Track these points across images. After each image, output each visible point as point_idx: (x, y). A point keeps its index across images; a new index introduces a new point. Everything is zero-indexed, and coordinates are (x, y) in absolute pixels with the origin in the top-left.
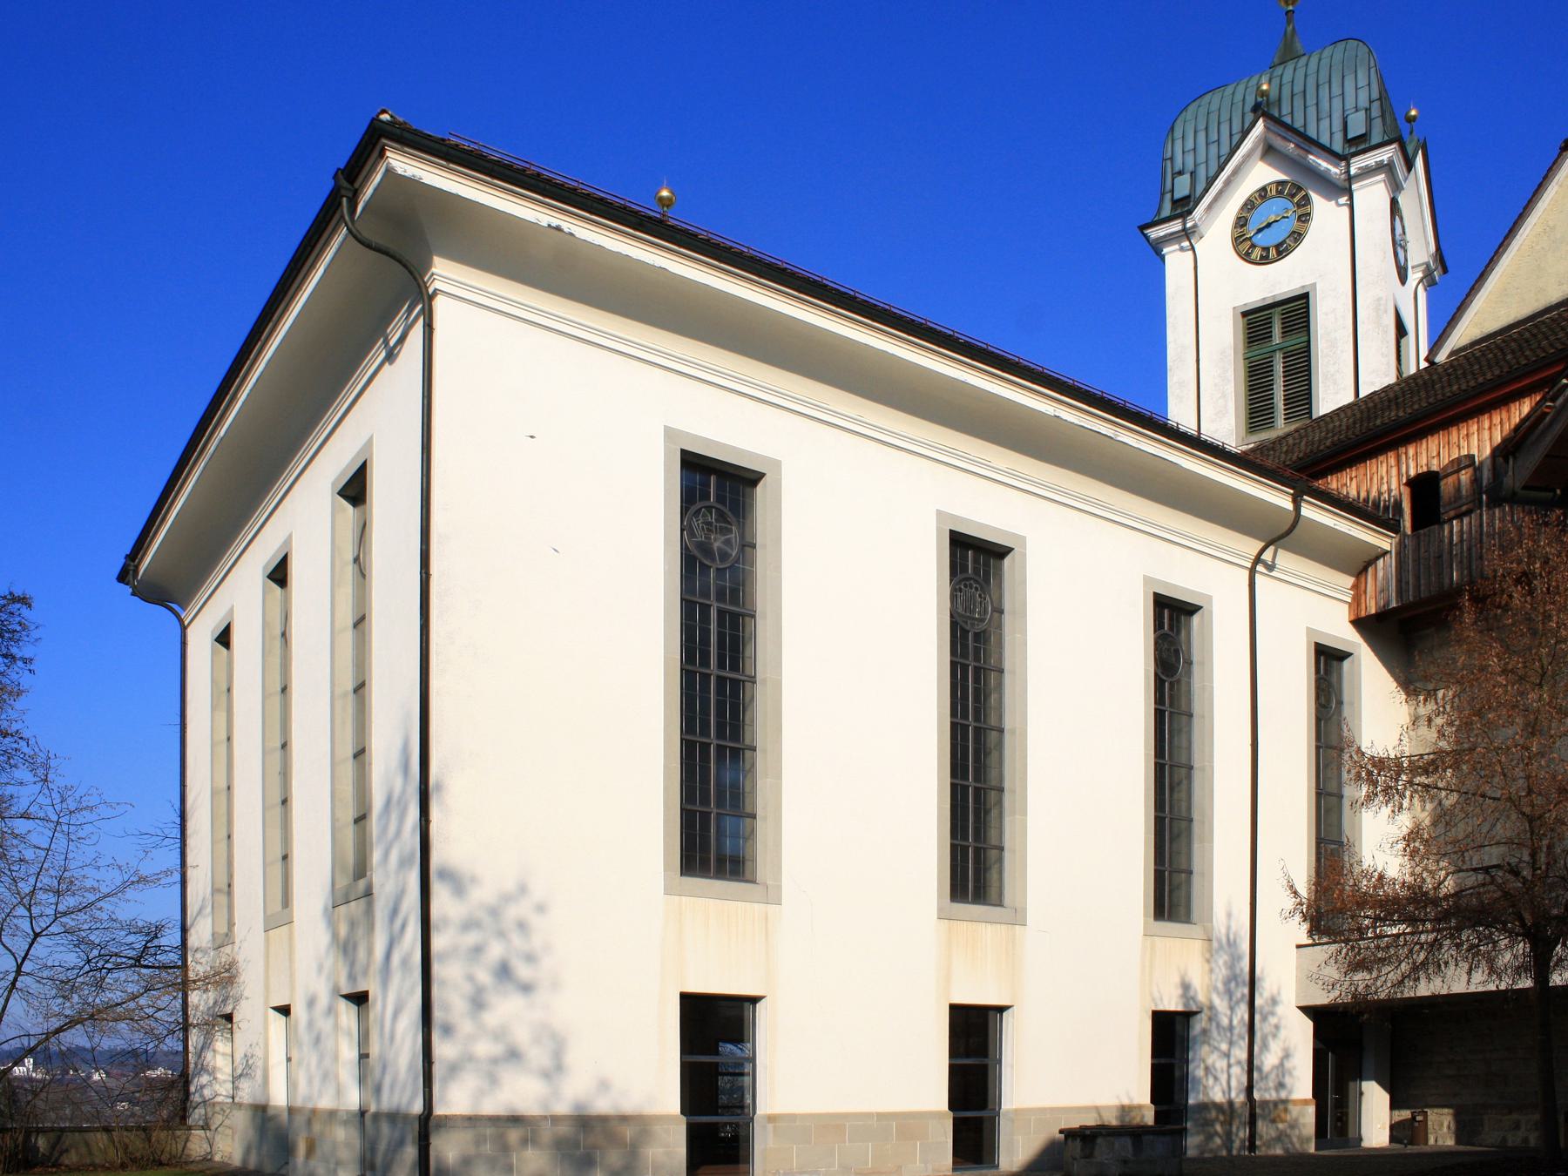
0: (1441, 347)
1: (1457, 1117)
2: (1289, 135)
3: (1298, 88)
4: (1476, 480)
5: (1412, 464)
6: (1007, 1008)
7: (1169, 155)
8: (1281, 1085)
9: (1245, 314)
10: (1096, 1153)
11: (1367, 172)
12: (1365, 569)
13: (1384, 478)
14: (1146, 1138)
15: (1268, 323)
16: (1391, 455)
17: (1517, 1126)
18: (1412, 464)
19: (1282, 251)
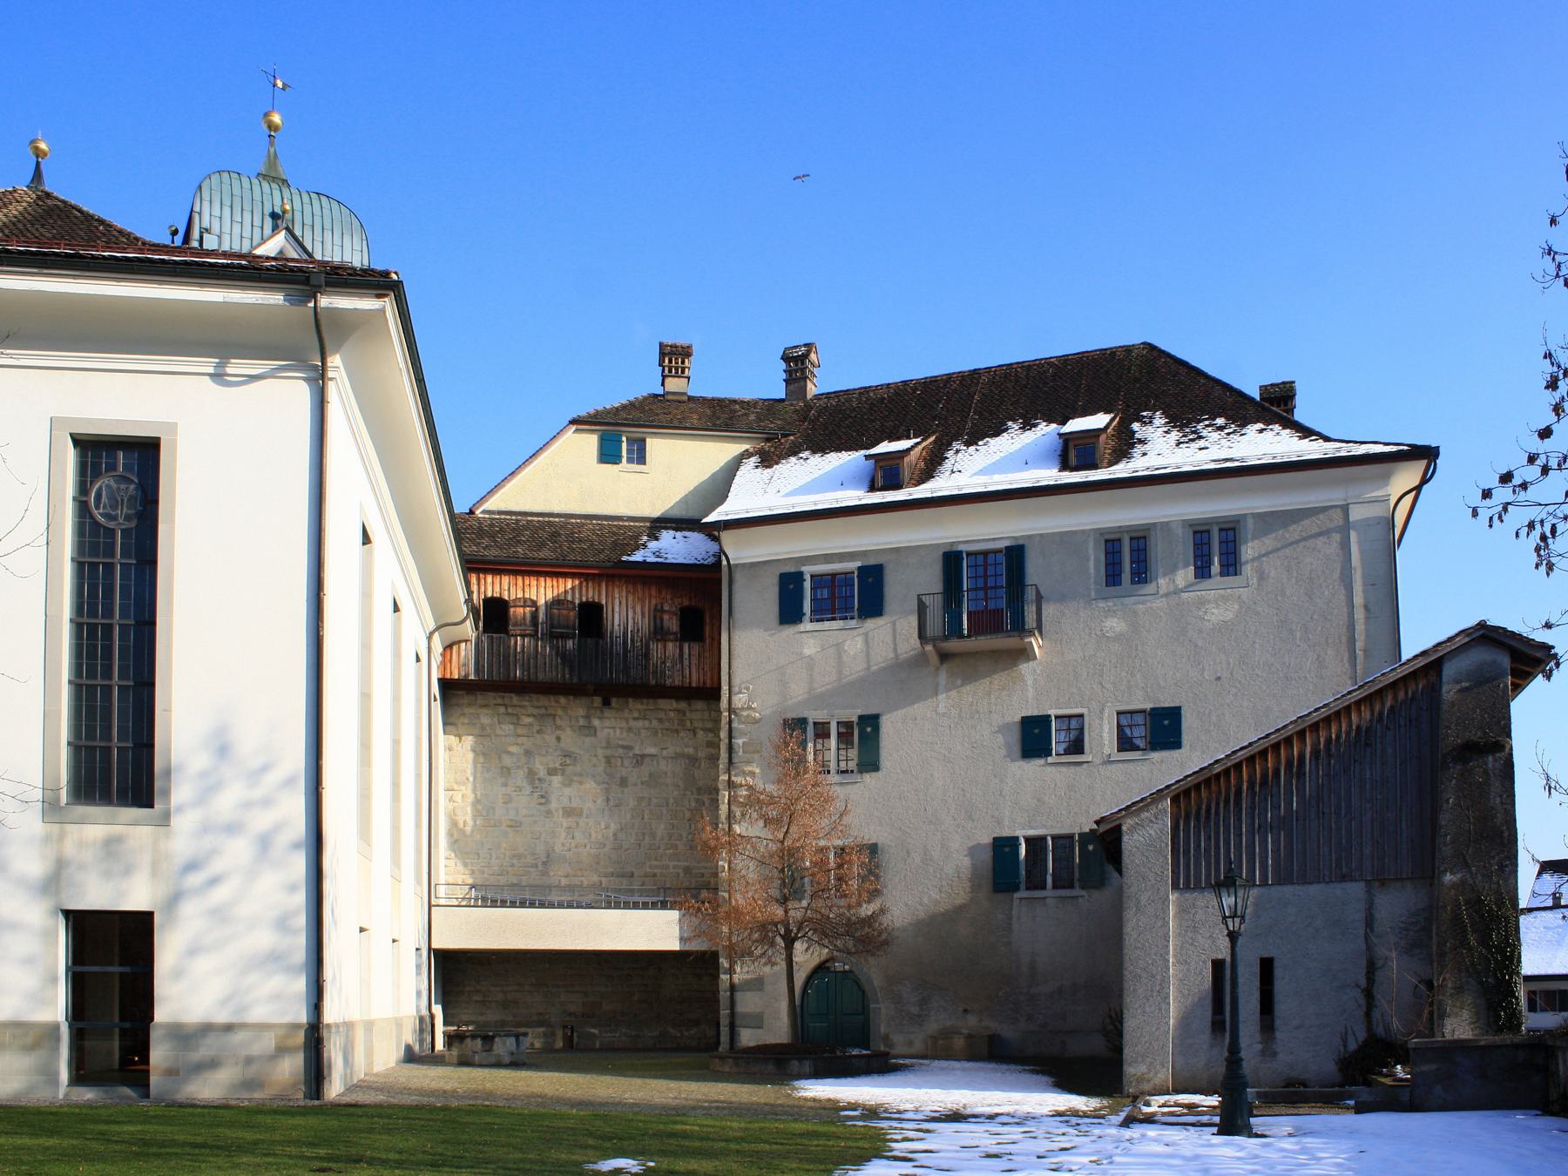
4: (535, 616)
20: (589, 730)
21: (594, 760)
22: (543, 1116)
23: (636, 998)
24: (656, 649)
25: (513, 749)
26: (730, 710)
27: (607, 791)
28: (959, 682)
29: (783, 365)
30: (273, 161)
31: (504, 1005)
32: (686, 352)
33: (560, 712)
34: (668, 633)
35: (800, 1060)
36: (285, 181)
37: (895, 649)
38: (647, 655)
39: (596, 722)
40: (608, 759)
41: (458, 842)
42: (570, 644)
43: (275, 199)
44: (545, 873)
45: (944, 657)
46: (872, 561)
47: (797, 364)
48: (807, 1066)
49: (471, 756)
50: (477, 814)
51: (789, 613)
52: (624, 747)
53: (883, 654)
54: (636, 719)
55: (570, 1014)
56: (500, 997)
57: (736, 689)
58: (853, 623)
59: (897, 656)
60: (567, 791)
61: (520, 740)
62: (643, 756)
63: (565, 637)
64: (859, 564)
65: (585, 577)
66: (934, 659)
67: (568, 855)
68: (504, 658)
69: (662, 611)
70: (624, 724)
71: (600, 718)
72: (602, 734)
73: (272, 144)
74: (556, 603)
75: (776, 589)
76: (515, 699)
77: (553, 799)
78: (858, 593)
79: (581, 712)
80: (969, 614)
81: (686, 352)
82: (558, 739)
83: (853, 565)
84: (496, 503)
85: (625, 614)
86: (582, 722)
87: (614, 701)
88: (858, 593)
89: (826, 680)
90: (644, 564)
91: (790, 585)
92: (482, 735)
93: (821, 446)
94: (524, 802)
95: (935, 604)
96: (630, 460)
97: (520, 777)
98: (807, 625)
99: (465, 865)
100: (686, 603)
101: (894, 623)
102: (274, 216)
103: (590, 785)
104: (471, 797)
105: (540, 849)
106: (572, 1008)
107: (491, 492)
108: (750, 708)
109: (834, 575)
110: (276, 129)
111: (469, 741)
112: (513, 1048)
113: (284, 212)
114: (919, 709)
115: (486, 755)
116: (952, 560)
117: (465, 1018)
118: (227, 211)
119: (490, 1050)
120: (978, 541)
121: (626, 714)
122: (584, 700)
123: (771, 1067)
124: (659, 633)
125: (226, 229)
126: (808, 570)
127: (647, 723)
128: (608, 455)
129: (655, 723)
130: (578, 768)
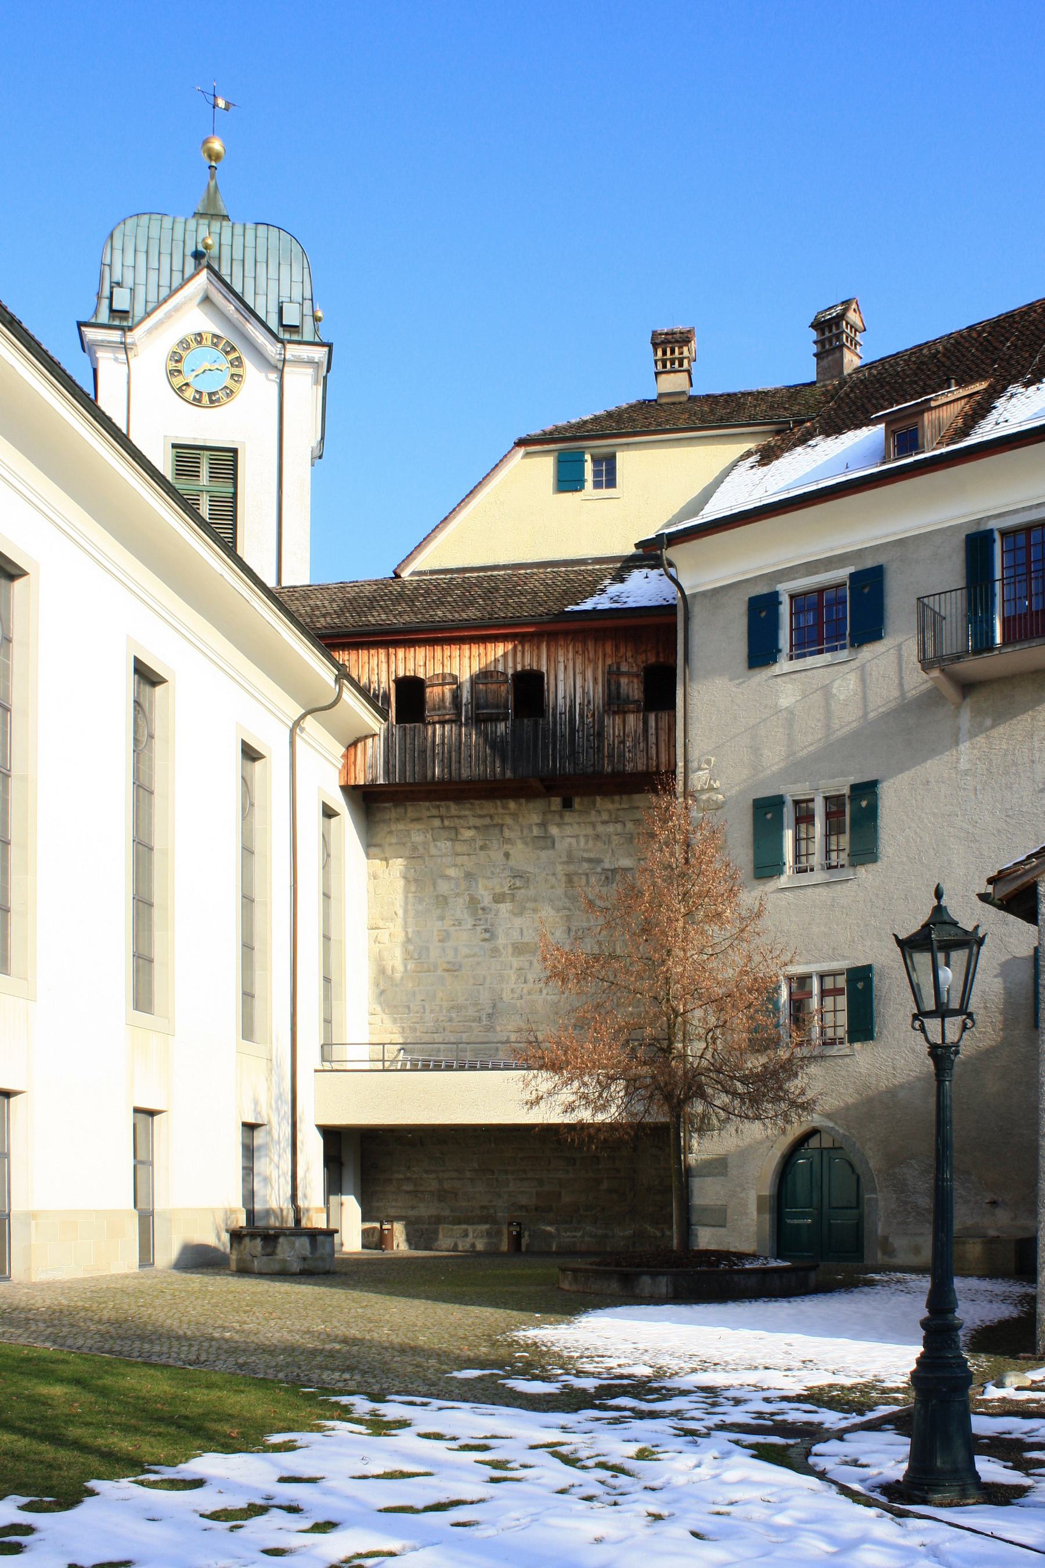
0: (407, 566)
1: (406, 1226)
2: (231, 297)
3: (238, 255)
4: (456, 697)
5: (401, 666)
6: (159, 1112)
7: (107, 261)
8: (266, 1202)
9: (174, 446)
10: (279, 1250)
11: (299, 362)
12: (354, 744)
13: (380, 668)
14: (320, 1238)
15: (197, 462)
16: (382, 652)
17: (466, 1235)
18: (401, 666)
19: (214, 400)
20: (546, 841)
21: (553, 880)
22: (44, 1360)
23: (605, 1186)
24: (613, 726)
25: (452, 872)
26: (686, 794)
27: (568, 918)
28: (988, 722)
29: (813, 335)
30: (212, 197)
31: (442, 1196)
32: (684, 339)
33: (509, 821)
34: (627, 700)
35: (654, 1275)
36: (226, 217)
37: (901, 685)
38: (600, 735)
39: (554, 830)
40: (570, 878)
41: (386, 990)
42: (501, 727)
43: (205, 234)
44: (490, 1029)
45: (967, 687)
46: (869, 563)
47: (830, 331)
48: (663, 1285)
49: (401, 883)
50: (408, 956)
51: (761, 652)
52: (590, 860)
53: (884, 694)
54: (604, 823)
55: (522, 1207)
56: (434, 1185)
57: (694, 765)
58: (843, 655)
59: (903, 693)
60: (518, 922)
61: (459, 860)
62: (614, 871)
63: (495, 719)
64: (852, 569)
65: (520, 639)
66: (950, 691)
67: (519, 1003)
68: (422, 754)
69: (619, 673)
70: (590, 831)
71: (559, 825)
72: (562, 846)
73: (212, 177)
74: (484, 676)
75: (744, 621)
76: (454, 809)
77: (500, 932)
78: (847, 612)
79: (536, 818)
80: (1005, 622)
81: (684, 339)
82: (507, 855)
83: (842, 574)
84: (428, 560)
85: (572, 681)
86: (536, 831)
87: (577, 802)
88: (847, 612)
89: (809, 739)
90: (595, 613)
91: (762, 610)
92: (414, 856)
93: (834, 428)
94: (465, 939)
95: (953, 608)
96: (597, 485)
97: (459, 908)
98: (784, 665)
99: (395, 1021)
100: (652, 660)
101: (899, 648)
102: (198, 255)
103: (547, 912)
104: (400, 937)
105: (485, 997)
106: (523, 1200)
107: (419, 547)
108: (711, 789)
109: (821, 591)
110: (217, 157)
111: (398, 865)
112: (307, 1251)
113: (207, 247)
114: (934, 767)
115: (419, 882)
116: (978, 544)
117: (392, 1212)
118: (141, 257)
119: (273, 1253)
120: (1015, 512)
121: (593, 816)
122: (539, 804)
123: (614, 1286)
124: (615, 703)
125: (141, 278)
126: (785, 588)
127: (619, 827)
128: (568, 480)
129: (630, 826)
130: (532, 892)
